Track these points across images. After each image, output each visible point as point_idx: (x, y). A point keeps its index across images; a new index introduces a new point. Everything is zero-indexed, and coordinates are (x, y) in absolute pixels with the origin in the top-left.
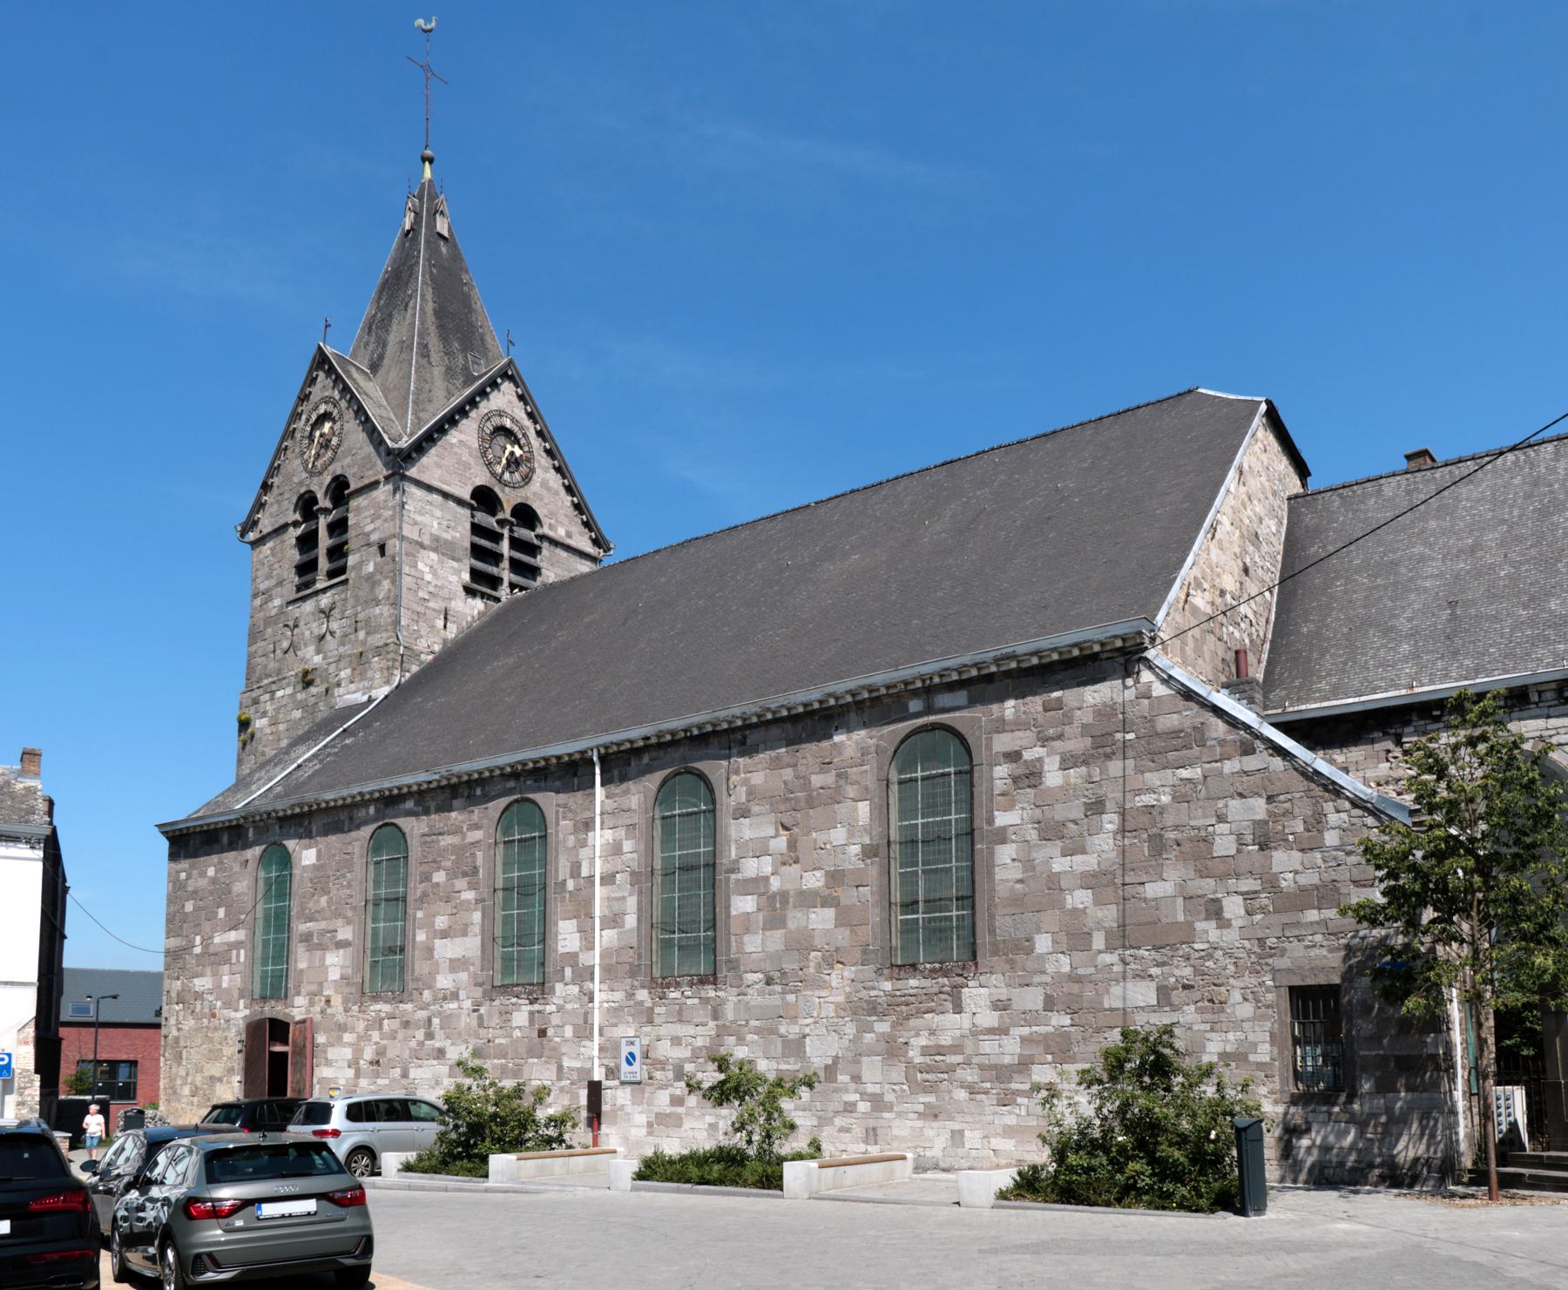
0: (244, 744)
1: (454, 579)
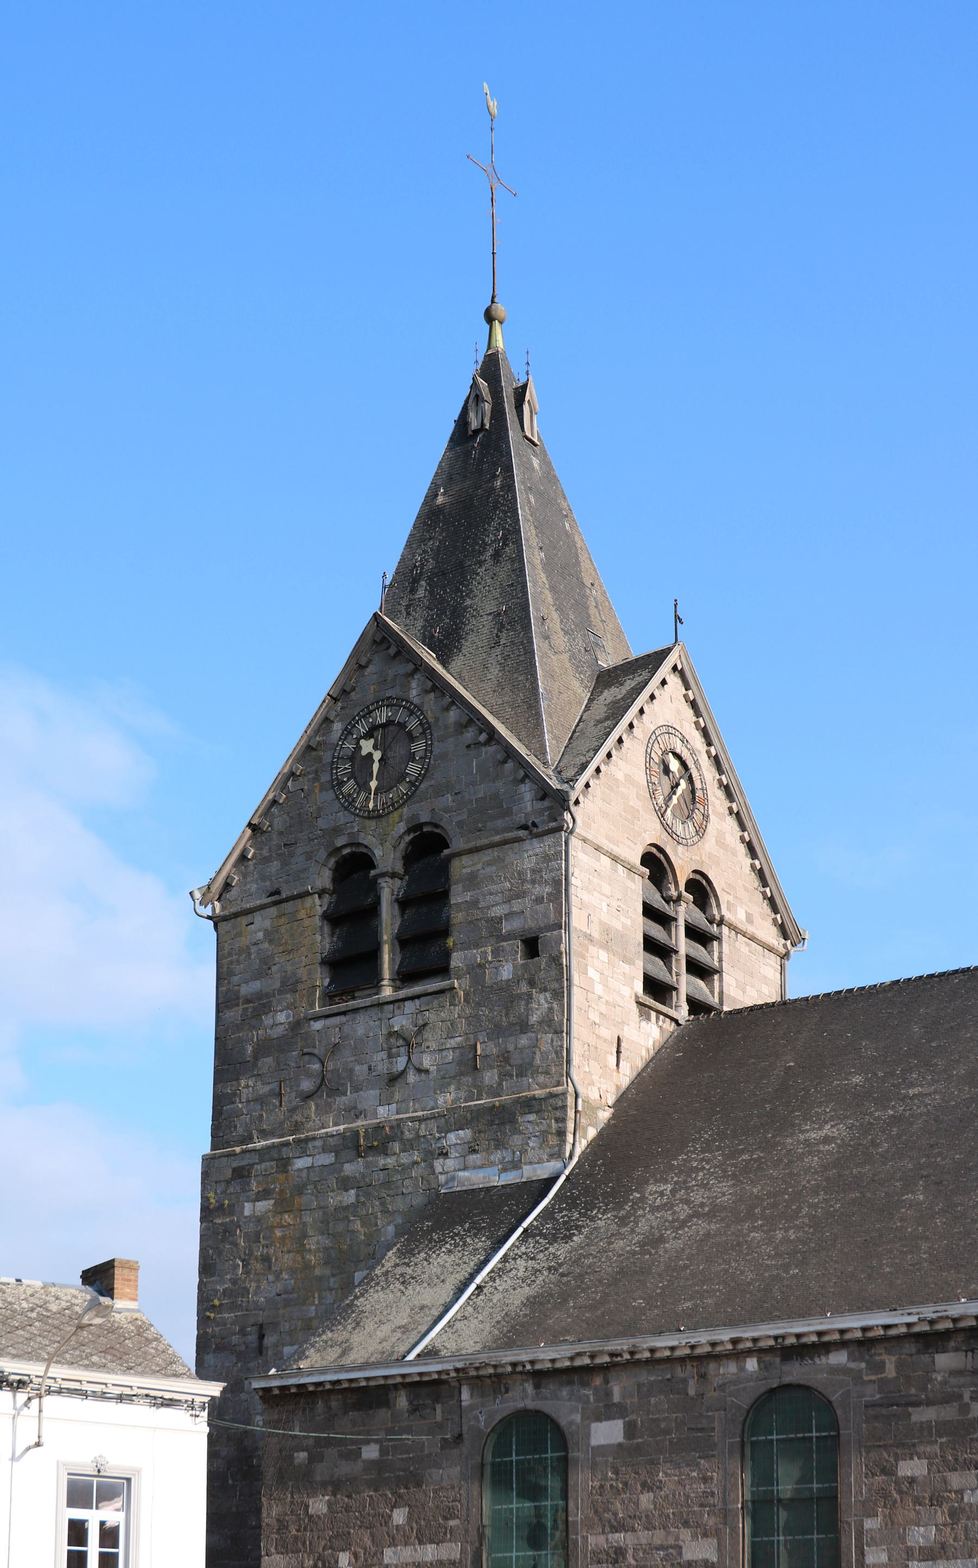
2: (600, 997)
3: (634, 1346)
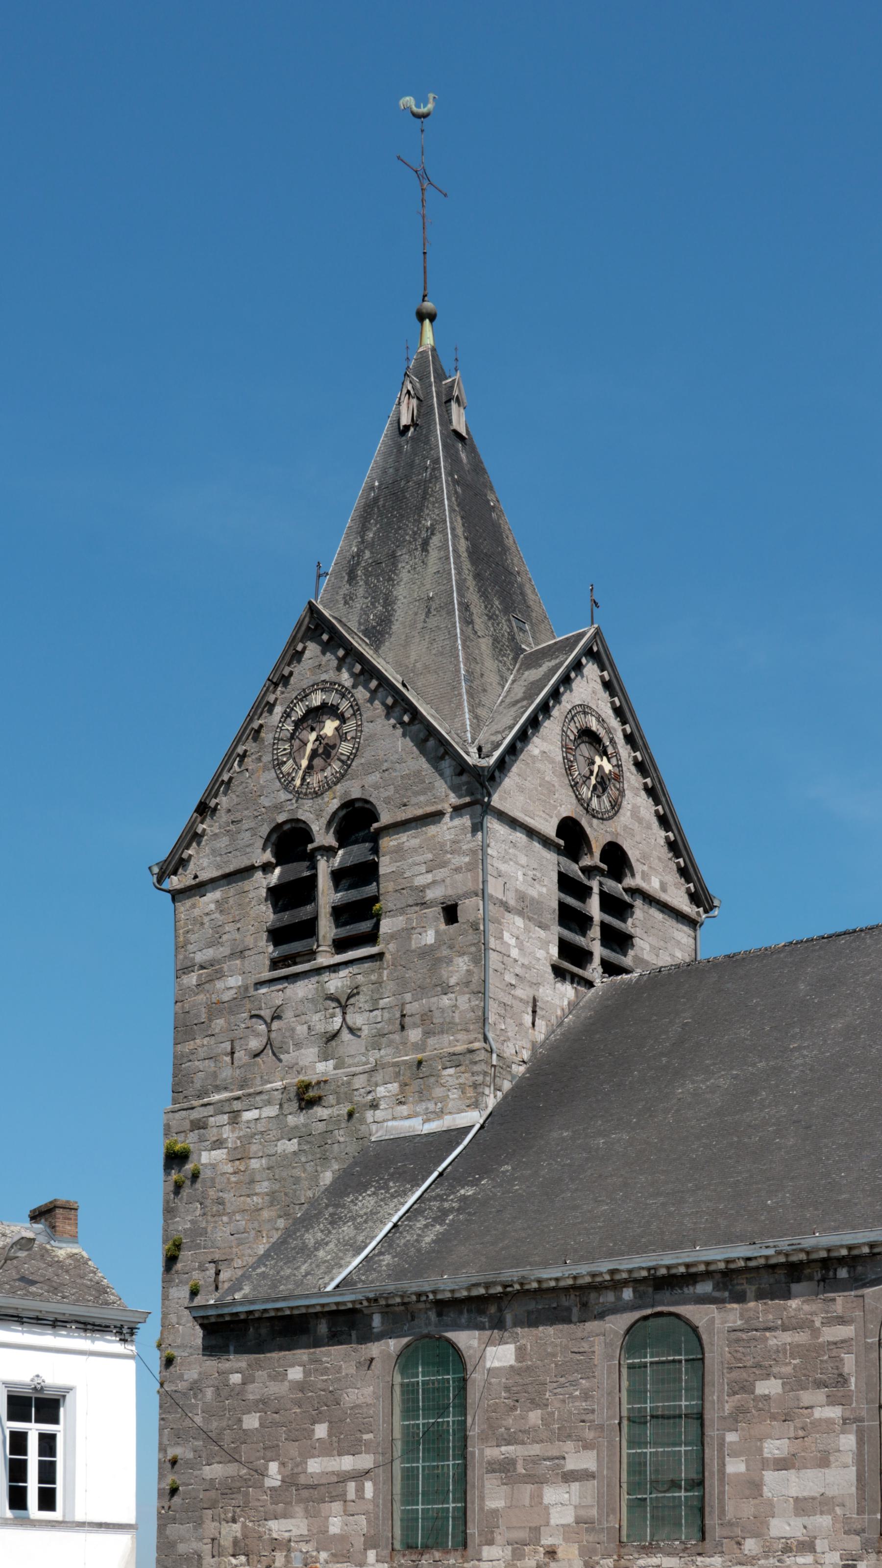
0: (178, 1187)
1: (541, 954)
3: (523, 1277)
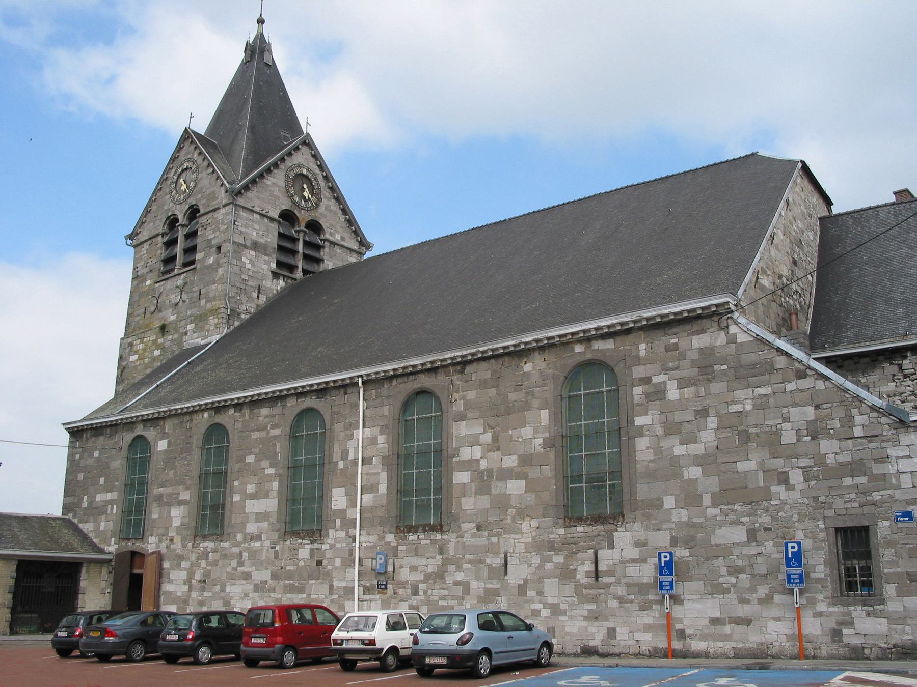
2: (249, 269)
